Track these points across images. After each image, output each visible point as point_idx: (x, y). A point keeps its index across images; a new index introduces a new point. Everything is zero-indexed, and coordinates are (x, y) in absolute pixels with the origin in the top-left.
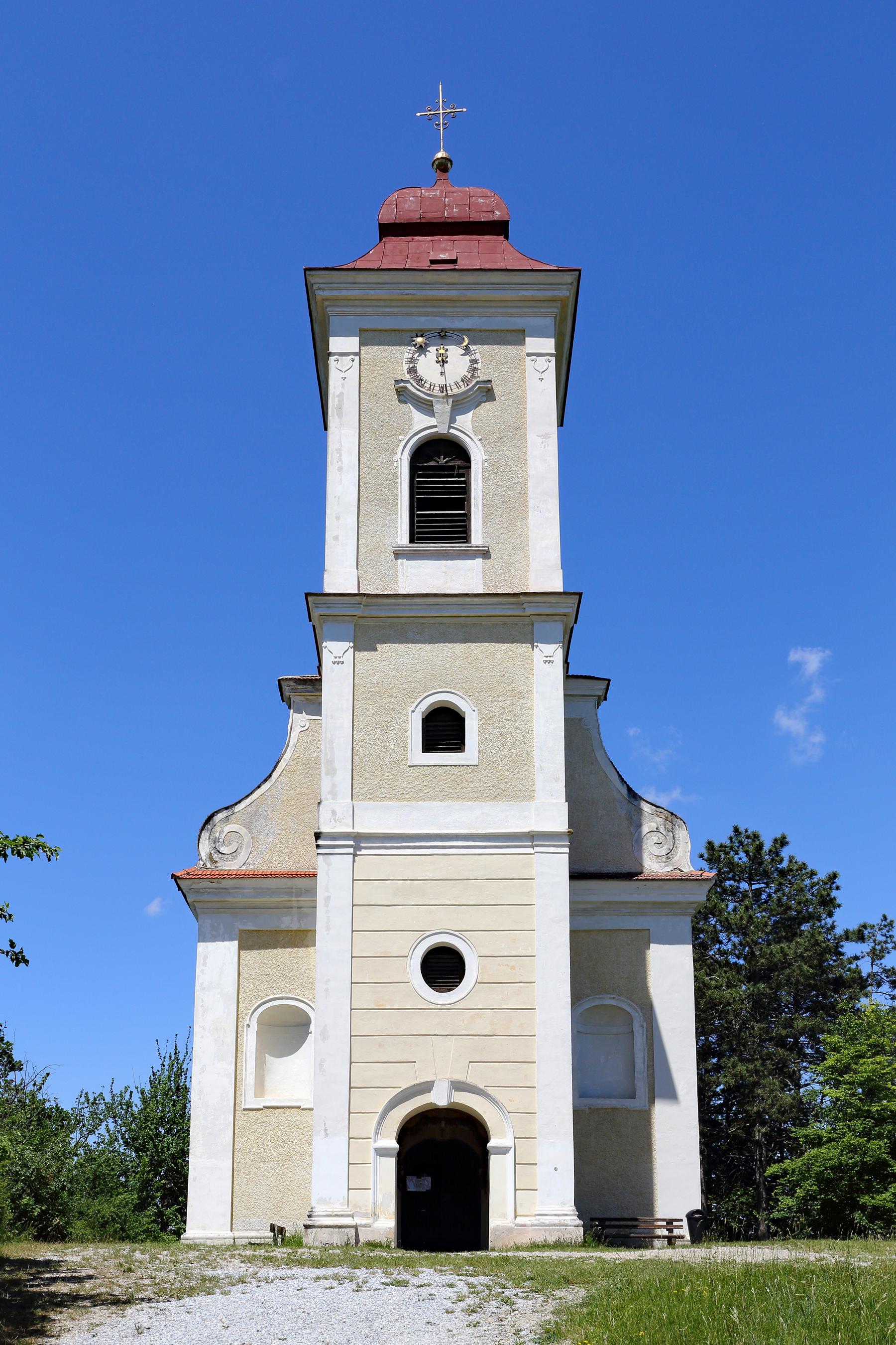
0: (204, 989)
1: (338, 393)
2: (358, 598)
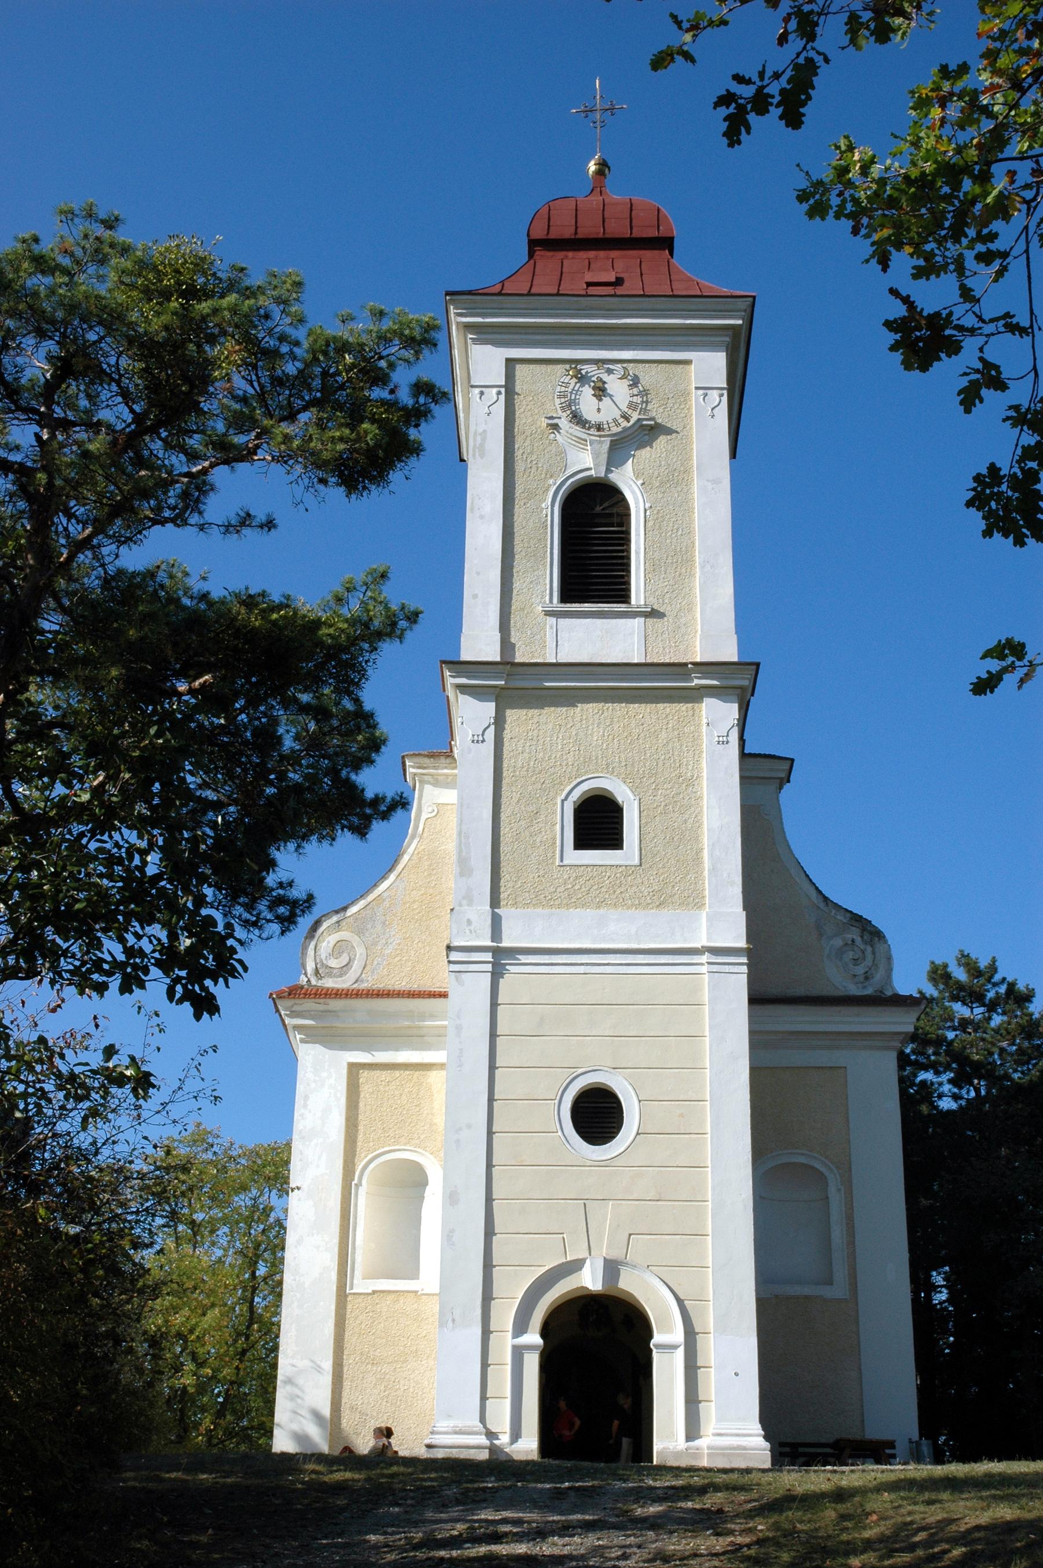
0: (303, 1138)
1: (480, 430)
2: (501, 667)
